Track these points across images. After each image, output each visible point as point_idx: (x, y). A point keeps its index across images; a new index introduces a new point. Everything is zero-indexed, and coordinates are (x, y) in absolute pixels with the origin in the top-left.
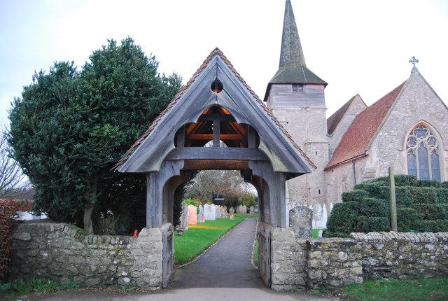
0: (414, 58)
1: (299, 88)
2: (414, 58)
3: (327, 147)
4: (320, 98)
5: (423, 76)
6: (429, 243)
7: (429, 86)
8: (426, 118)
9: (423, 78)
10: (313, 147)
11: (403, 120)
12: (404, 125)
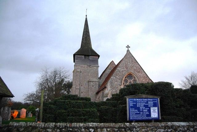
0: (128, 46)
1: (87, 57)
2: (128, 46)
3: (98, 83)
4: (96, 62)
5: (131, 53)
6: (49, 128)
7: (134, 58)
8: (132, 71)
9: (131, 54)
10: (92, 83)
11: (122, 72)
12: (122, 74)
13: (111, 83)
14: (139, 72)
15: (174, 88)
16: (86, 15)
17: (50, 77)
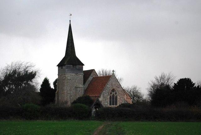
1: (75, 66)
3: (83, 89)
8: (115, 87)
13: (103, 94)
14: (119, 88)
15: (172, 85)
16: (70, 21)
17: (134, 90)
